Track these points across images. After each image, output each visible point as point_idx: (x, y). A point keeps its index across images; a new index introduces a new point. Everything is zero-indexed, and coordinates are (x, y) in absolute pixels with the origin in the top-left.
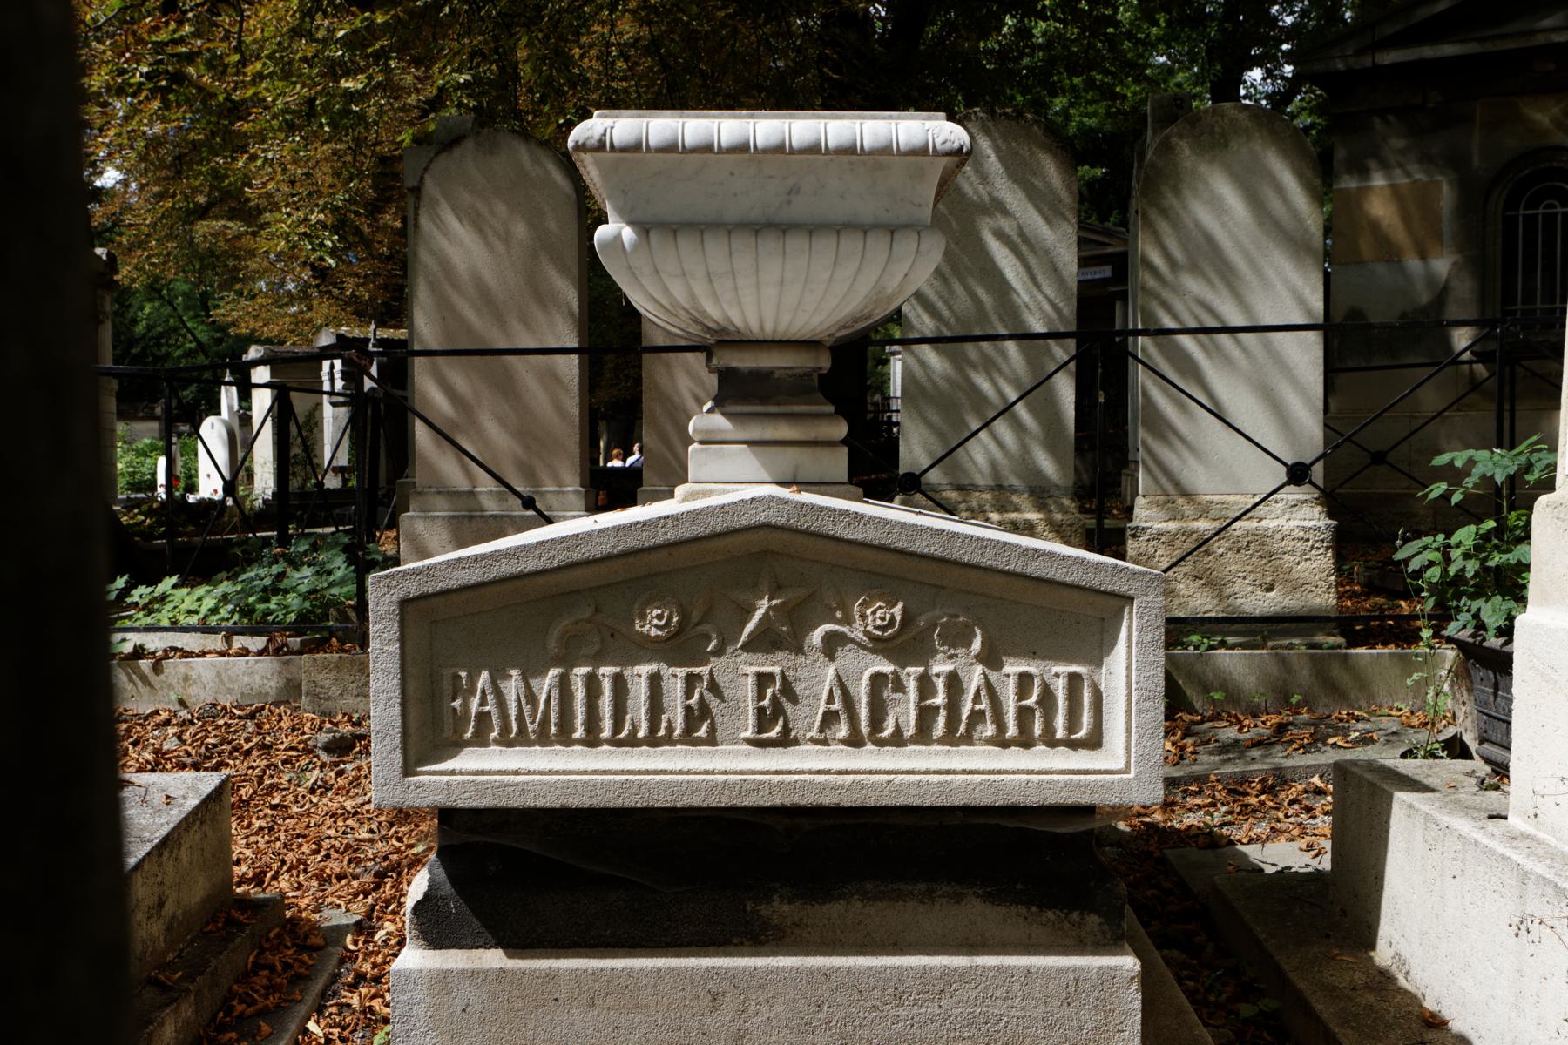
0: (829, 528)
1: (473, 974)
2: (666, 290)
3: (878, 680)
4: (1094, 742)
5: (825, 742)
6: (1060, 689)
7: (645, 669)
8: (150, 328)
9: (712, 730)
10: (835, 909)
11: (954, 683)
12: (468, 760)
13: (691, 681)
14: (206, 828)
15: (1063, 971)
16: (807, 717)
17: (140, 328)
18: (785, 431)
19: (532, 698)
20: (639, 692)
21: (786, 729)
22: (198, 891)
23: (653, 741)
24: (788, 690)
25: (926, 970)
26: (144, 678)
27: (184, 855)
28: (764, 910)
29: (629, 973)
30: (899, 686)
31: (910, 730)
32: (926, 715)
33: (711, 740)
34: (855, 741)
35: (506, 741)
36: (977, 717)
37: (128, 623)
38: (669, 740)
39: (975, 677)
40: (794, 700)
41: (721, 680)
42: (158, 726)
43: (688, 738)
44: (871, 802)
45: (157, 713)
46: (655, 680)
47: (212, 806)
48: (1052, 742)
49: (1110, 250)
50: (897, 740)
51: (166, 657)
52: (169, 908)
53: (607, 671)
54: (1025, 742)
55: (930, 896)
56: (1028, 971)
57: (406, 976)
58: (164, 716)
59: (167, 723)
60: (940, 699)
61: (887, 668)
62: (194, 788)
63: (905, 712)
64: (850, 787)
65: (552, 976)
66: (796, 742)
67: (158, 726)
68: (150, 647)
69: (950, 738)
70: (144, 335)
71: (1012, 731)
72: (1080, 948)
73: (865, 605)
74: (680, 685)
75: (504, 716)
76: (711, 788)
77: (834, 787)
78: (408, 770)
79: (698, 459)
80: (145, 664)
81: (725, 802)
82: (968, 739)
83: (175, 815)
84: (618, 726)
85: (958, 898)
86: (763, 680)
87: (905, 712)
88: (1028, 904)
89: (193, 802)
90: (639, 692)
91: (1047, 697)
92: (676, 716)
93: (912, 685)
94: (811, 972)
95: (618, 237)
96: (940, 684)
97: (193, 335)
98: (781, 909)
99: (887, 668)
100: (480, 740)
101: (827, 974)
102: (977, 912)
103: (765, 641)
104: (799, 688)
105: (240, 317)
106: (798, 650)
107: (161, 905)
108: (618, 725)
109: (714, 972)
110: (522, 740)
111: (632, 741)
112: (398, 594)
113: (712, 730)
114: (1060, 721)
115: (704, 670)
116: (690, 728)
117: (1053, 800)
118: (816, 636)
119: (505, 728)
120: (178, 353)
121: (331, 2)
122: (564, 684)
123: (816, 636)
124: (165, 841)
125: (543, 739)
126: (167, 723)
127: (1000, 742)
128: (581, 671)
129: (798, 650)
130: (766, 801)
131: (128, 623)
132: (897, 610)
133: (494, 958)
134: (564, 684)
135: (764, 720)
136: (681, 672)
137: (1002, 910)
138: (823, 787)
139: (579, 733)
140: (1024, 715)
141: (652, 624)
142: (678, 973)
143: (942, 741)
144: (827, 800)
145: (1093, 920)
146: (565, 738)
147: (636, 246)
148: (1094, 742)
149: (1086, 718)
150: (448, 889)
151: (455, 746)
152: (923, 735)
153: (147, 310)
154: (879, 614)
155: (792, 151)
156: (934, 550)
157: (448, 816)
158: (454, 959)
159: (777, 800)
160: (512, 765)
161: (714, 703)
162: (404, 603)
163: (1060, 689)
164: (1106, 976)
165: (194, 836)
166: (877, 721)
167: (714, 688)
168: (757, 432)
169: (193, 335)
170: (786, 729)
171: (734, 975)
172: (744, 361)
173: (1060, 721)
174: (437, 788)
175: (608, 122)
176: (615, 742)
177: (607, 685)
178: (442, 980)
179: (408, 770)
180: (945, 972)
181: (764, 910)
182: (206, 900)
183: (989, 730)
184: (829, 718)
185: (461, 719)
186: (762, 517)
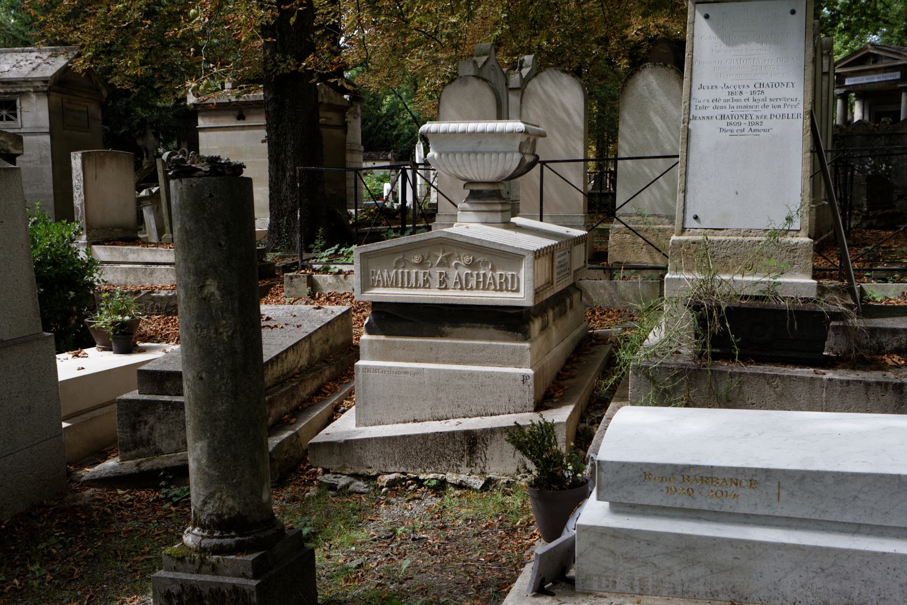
0: (454, 238)
1: (378, 341)
2: (447, 170)
3: (467, 274)
4: (517, 291)
5: (455, 289)
6: (509, 277)
7: (414, 271)
8: (388, 110)
9: (430, 285)
10: (459, 329)
11: (484, 275)
12: (376, 291)
13: (425, 273)
14: (343, 321)
15: (511, 346)
16: (451, 283)
17: (384, 110)
18: (484, 208)
19: (389, 277)
20: (413, 276)
21: (446, 286)
22: (340, 340)
23: (416, 287)
24: (446, 276)
25: (480, 344)
26: (341, 281)
27: (335, 327)
28: (443, 329)
29: (412, 342)
30: (472, 275)
31: (474, 287)
32: (478, 283)
33: (429, 288)
34: (462, 289)
35: (383, 286)
36: (490, 284)
37: (337, 262)
38: (420, 287)
39: (489, 275)
40: (448, 279)
41: (432, 274)
42: (345, 298)
43: (424, 287)
44: (464, 303)
45: (345, 293)
46: (417, 273)
47: (345, 315)
48: (507, 290)
49: (899, 63)
50: (471, 289)
51: (349, 274)
52: (330, 342)
53: (406, 271)
54: (501, 290)
55: (481, 327)
56: (503, 346)
57: (363, 340)
58: (348, 294)
59: (348, 297)
60: (481, 280)
61: (469, 272)
62: (340, 310)
63: (473, 282)
64: (459, 300)
65: (395, 342)
66: (448, 289)
67: (345, 298)
68: (344, 270)
69: (484, 289)
70: (385, 114)
71: (498, 288)
72: (517, 340)
73: (464, 256)
74: (422, 275)
75: (383, 281)
76: (428, 299)
77: (456, 300)
78: (362, 293)
79: (461, 216)
80: (342, 276)
81: (431, 302)
82: (488, 289)
83: (333, 316)
84: (408, 284)
85: (488, 328)
86: (441, 274)
87: (473, 282)
88: (504, 330)
89: (339, 313)
90: (413, 276)
91: (506, 279)
92: (421, 281)
93: (475, 276)
94: (453, 344)
95: (433, 156)
96: (482, 276)
97: (410, 112)
98: (447, 329)
99: (469, 272)
100: (378, 286)
101: (456, 344)
102: (492, 331)
103: (441, 264)
104: (449, 276)
105: (426, 109)
106: (449, 267)
107: (328, 340)
108: (408, 284)
109: (431, 343)
110: (387, 286)
111: (411, 287)
112: (360, 252)
113: (430, 285)
114: (510, 285)
115: (428, 271)
116: (424, 285)
117: (506, 304)
118: (453, 264)
119: (384, 284)
120: (402, 122)
121: (3, 582)
122: (396, 273)
123: (453, 264)
124: (329, 323)
125: (392, 286)
126: (348, 297)
127: (495, 290)
128: (400, 271)
129: (449, 267)
130: (440, 302)
131: (337, 262)
132: (471, 258)
133: (382, 338)
134: (396, 273)
135: (441, 283)
136: (423, 271)
137: (498, 331)
138: (454, 299)
139: (400, 285)
140: (501, 283)
141: (416, 260)
142: (423, 342)
143: (482, 289)
144: (454, 302)
145: (520, 335)
146: (397, 286)
147: (438, 158)
148: (517, 291)
149: (516, 285)
150: (373, 321)
151: (373, 287)
152: (477, 288)
153: (388, 99)
154: (467, 259)
155: (477, 133)
156: (479, 244)
157: (374, 304)
158: (374, 337)
159: (443, 302)
160: (392, 292)
161: (430, 279)
162: (361, 254)
163: (509, 277)
164: (522, 349)
165: (339, 323)
166: (467, 284)
167: (430, 275)
168: (476, 208)
169: (410, 112)
170: (446, 286)
171: (436, 344)
172: (475, 188)
173: (510, 285)
174: (368, 297)
175: (430, 125)
176: (407, 287)
177: (406, 274)
178: (371, 341)
179: (362, 293)
180: (484, 345)
181: (443, 329)
182: (343, 343)
183: (493, 287)
184: (456, 283)
185: (374, 281)
186: (439, 235)
